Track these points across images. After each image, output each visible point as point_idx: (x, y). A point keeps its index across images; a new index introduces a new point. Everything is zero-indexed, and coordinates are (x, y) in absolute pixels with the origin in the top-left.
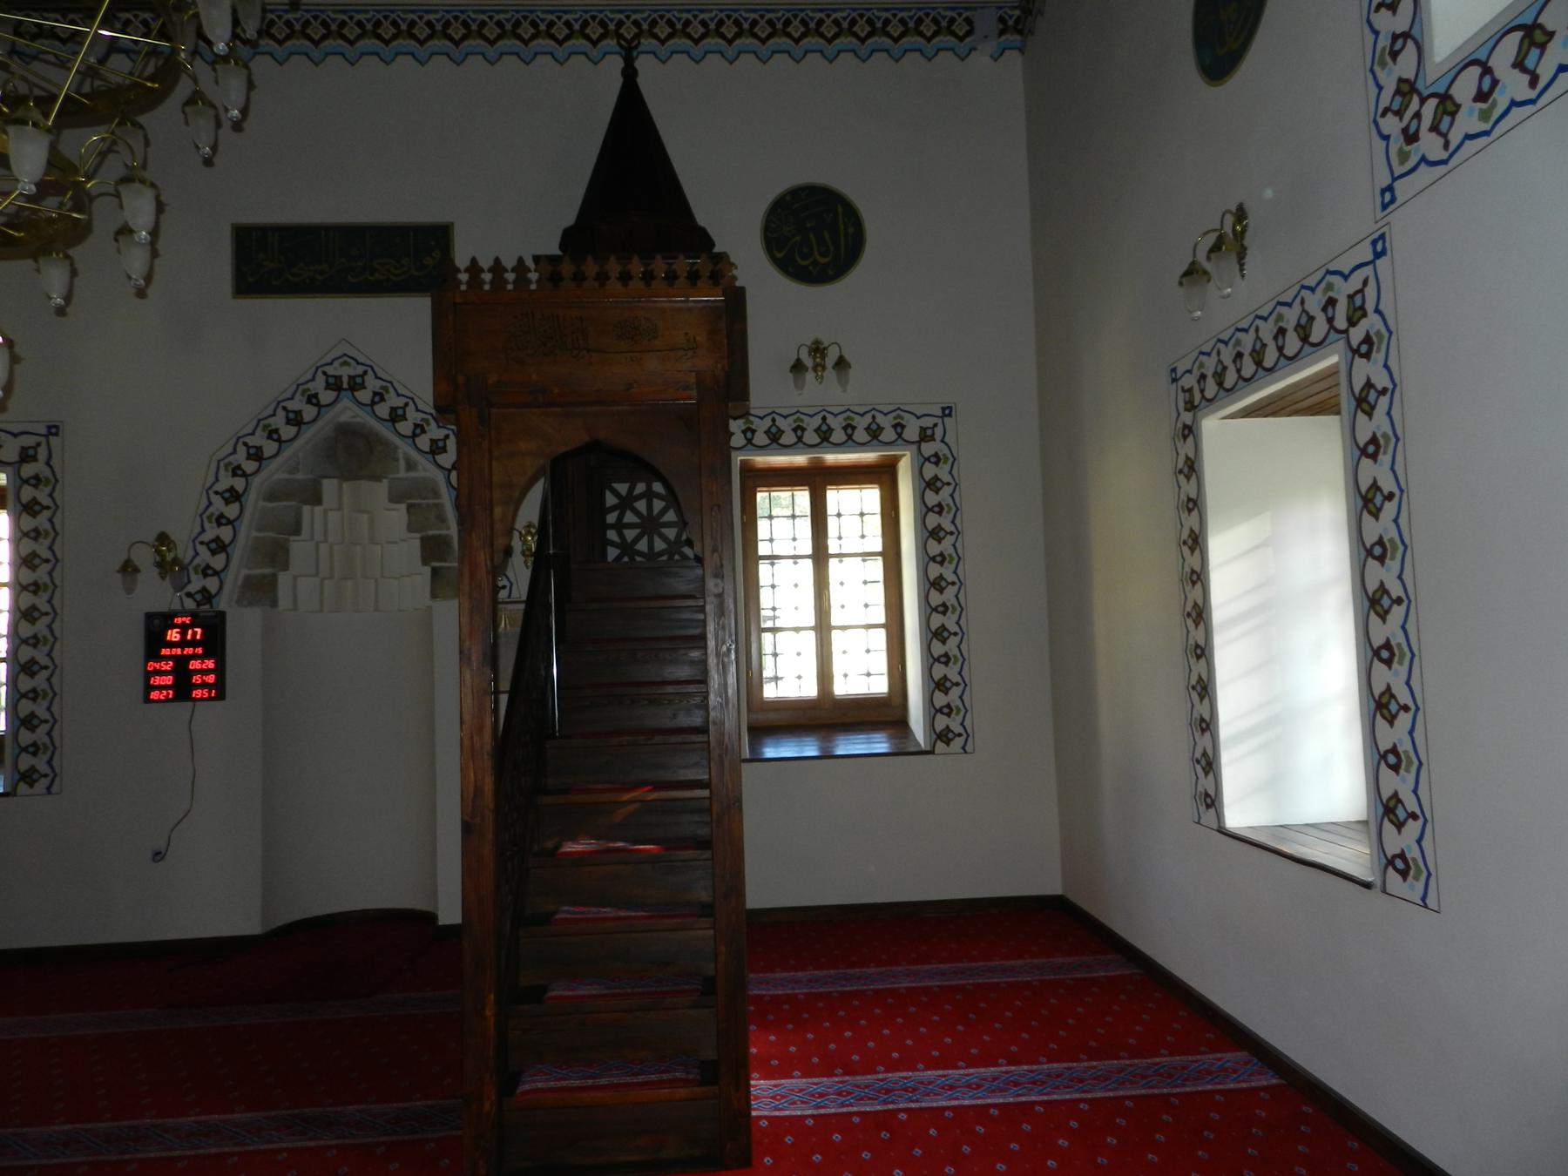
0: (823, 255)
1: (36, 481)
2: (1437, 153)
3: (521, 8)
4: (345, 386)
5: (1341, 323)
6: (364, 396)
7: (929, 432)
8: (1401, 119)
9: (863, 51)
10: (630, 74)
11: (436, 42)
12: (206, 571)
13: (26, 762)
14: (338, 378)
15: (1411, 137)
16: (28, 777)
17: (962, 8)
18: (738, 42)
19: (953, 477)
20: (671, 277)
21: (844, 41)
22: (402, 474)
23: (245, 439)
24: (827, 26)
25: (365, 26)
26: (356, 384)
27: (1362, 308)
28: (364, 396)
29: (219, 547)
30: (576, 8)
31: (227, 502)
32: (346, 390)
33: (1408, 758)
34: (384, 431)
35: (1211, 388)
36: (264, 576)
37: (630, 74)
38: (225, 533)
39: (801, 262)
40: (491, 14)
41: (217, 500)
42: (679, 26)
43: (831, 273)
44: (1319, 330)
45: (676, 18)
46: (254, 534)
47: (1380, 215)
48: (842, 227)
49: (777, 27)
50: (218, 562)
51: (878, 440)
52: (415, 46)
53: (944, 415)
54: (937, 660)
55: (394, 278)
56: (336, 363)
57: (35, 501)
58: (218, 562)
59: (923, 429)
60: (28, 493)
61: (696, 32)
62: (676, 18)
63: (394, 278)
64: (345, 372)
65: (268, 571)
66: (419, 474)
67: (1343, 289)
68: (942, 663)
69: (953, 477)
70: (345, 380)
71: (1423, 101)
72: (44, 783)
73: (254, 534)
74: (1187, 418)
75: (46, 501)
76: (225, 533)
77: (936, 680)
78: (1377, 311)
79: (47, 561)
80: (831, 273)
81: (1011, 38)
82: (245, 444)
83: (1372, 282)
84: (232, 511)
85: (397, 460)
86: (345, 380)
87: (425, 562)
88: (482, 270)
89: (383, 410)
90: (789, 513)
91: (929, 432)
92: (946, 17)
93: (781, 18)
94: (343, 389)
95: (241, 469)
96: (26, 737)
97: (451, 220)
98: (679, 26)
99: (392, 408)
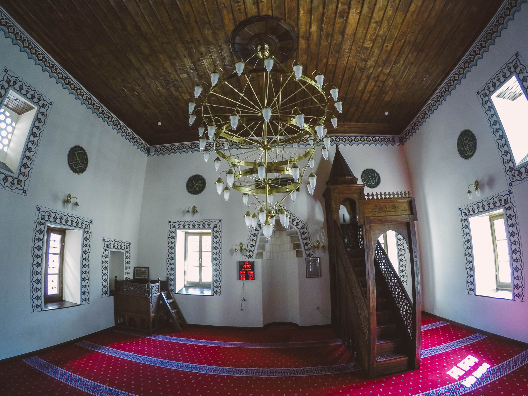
0: (373, 182)
1: (217, 232)
2: (519, 179)
5: (503, 203)
7: (216, 226)
10: (337, 148)
12: (250, 251)
13: (215, 289)
15: (514, 176)
16: (216, 292)
18: (352, 142)
27: (508, 201)
29: (252, 246)
33: (519, 260)
35: (471, 212)
36: (261, 252)
37: (337, 148)
38: (254, 243)
41: (252, 236)
42: (341, 139)
44: (498, 204)
46: (259, 243)
47: (509, 187)
50: (252, 249)
57: (216, 236)
58: (252, 249)
59: (173, 227)
60: (215, 234)
65: (262, 251)
66: (293, 230)
67: (503, 199)
71: (515, 171)
72: (219, 294)
73: (259, 243)
74: (465, 218)
75: (218, 236)
76: (254, 243)
78: (511, 202)
79: (219, 248)
83: (509, 197)
84: (255, 238)
87: (294, 249)
88: (391, 194)
90: (273, 243)
91: (216, 226)
96: (215, 284)
98: (341, 139)
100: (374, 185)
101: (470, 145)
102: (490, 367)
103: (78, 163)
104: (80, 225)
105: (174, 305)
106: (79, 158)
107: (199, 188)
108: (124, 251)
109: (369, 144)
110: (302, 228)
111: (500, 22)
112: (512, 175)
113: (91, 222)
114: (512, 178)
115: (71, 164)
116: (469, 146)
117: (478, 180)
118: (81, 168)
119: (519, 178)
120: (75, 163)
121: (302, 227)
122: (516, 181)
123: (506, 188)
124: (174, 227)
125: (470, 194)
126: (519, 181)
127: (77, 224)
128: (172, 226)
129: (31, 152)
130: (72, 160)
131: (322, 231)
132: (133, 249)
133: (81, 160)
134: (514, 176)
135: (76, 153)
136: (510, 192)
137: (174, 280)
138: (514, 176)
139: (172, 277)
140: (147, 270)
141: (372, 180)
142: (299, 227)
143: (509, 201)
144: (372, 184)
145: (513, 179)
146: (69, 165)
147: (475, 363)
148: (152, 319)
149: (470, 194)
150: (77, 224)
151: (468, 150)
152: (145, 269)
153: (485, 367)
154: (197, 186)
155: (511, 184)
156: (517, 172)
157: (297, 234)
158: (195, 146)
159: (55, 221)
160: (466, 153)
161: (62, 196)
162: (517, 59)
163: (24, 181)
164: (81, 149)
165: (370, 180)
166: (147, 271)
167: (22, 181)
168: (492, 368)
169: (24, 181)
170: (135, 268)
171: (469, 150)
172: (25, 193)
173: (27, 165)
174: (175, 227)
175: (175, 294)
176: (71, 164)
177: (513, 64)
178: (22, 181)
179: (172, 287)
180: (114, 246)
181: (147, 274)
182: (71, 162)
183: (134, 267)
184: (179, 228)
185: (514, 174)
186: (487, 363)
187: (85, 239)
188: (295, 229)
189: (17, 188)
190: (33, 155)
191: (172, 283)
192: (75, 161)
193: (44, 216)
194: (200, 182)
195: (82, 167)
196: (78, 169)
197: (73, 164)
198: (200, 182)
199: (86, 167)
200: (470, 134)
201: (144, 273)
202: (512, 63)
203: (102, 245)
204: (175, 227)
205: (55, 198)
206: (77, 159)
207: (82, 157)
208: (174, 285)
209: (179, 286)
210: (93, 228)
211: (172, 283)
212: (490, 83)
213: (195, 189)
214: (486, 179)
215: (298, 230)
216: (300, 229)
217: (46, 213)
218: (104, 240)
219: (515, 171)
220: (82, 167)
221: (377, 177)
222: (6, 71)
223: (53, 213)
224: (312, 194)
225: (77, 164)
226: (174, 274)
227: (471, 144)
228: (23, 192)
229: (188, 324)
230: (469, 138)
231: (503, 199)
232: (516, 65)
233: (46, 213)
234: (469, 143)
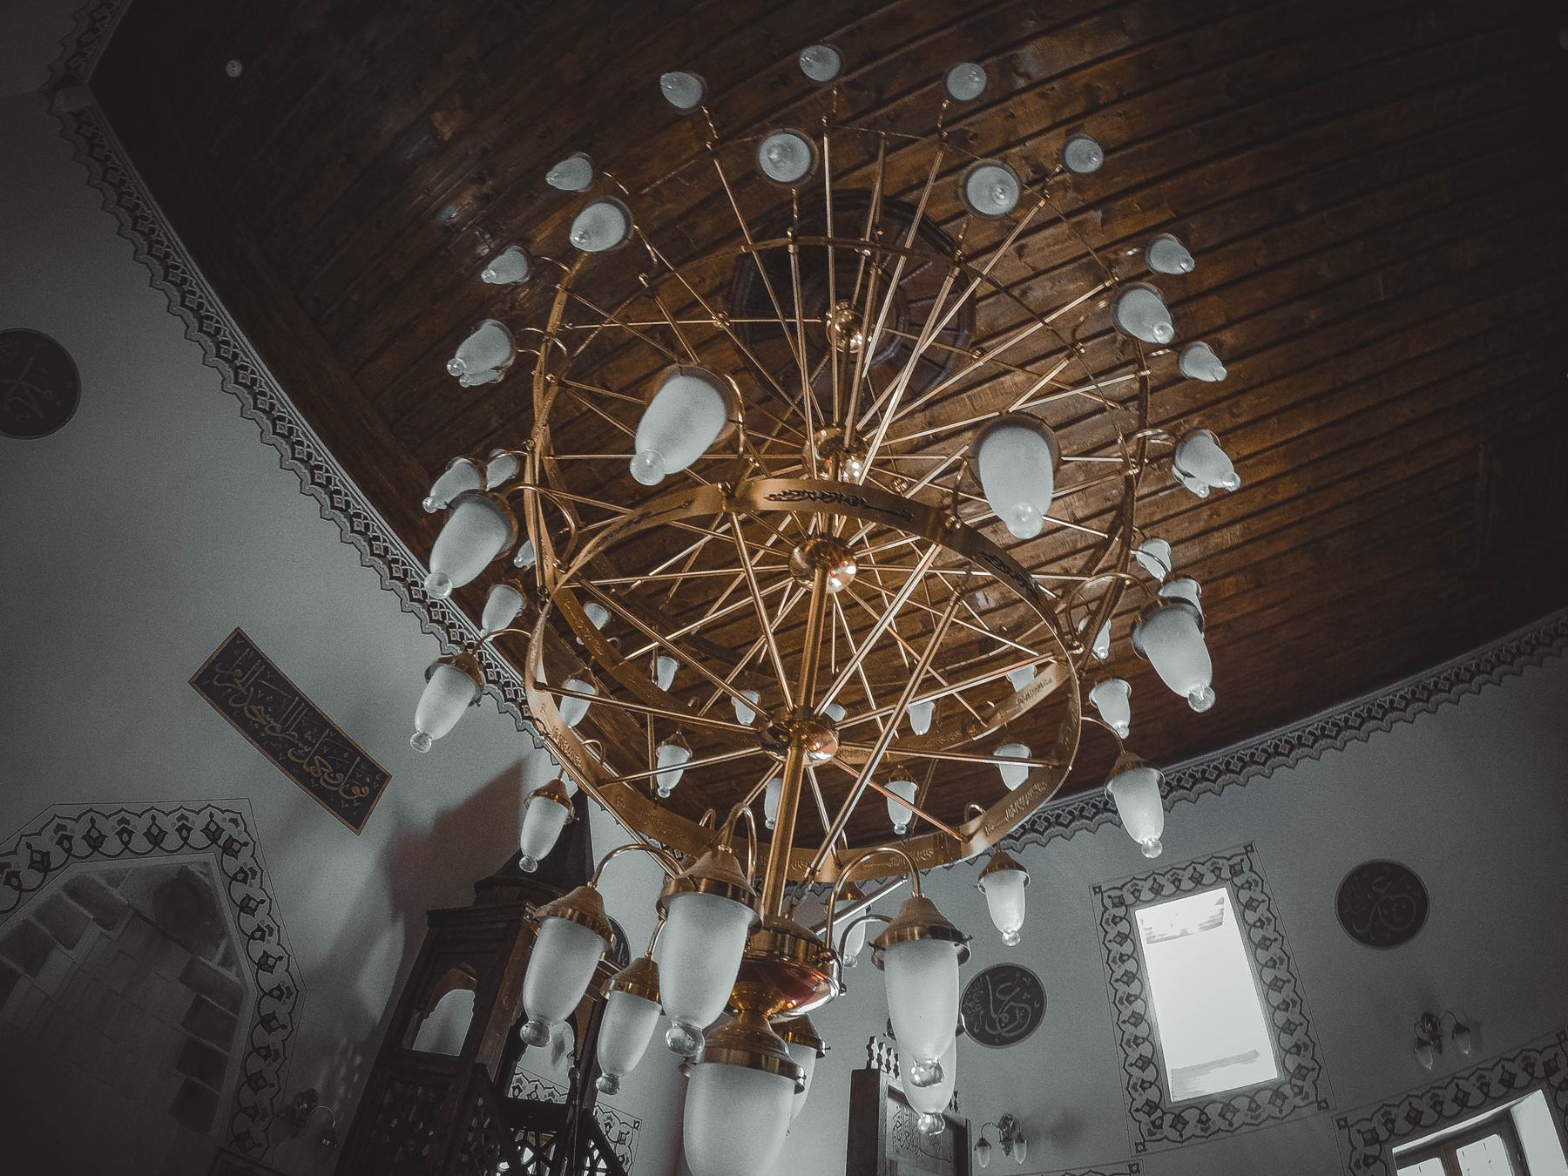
4: (220, 843)
6: (232, 865)
8: (1150, 1116)
14: (220, 830)
19: (1188, 866)
20: (246, 906)
22: (213, 964)
23: (96, 816)
25: (369, 531)
26: (230, 849)
28: (232, 865)
31: (1143, 1069)
32: (219, 846)
34: (229, 914)
46: (32, 919)
47: (1140, 1163)
53: (1247, 852)
55: (324, 784)
56: (228, 816)
63: (324, 784)
64: (229, 830)
66: (230, 974)
69: (1188, 866)
70: (225, 837)
71: (1164, 1113)
73: (32, 919)
82: (93, 821)
85: (218, 946)
86: (225, 837)
89: (240, 891)
93: (209, 312)
94: (217, 844)
95: (1393, 1124)
99: (1406, 1118)
110: (276, 993)
111: (1061, 820)
116: (1011, 1011)
121: (279, 988)
125: (983, 1151)
126: (1170, 1140)
131: (353, 1059)
138: (1156, 1126)
142: (268, 979)
143: (1118, 893)
149: (983, 1151)
155: (1141, 1147)
156: (1169, 1118)
157: (236, 1005)
162: (1105, 894)
171: (1007, 1025)
177: (1231, 862)
188: (240, 974)
202: (1228, 859)
212: (1184, 869)
215: (253, 994)
216: (265, 994)
219: (1164, 1113)
224: (530, 861)
227: (1020, 1009)
232: (1238, 868)
234: (1015, 1005)
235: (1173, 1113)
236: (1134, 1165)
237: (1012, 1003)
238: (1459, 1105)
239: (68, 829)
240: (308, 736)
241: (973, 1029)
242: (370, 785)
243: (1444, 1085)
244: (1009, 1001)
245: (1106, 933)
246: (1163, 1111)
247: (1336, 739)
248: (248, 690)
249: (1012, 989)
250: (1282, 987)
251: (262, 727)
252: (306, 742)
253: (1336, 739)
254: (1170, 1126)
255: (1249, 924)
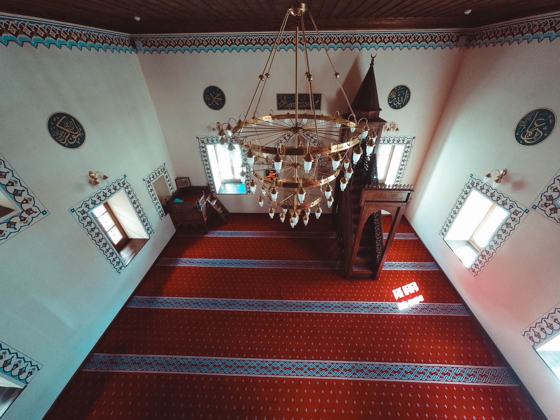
0: (400, 103)
3: (260, 35)
5: (122, 185)
8: (546, 201)
9: (262, 49)
11: (192, 46)
17: (439, 32)
21: (249, 45)
24: (286, 40)
30: (191, 36)
39: (394, 104)
40: (188, 38)
43: (400, 107)
45: (249, 38)
48: (406, 96)
49: (168, 43)
51: (91, 221)
52: (156, 48)
54: (497, 200)
61: (205, 44)
62: (249, 38)
67: (121, 182)
68: (499, 200)
71: (552, 204)
77: (502, 204)
78: (519, 218)
80: (400, 107)
81: (250, 46)
83: (125, 180)
92: (367, 36)
93: (409, 36)
97: (276, 94)
100: (399, 105)
101: (537, 133)
102: (423, 302)
103: (71, 134)
104: (118, 187)
105: (219, 204)
106: (67, 128)
107: (219, 102)
108: (163, 174)
109: (336, 48)
112: (546, 203)
113: (125, 176)
114: (542, 204)
115: (64, 143)
116: (534, 133)
117: (508, 172)
118: (79, 137)
119: (548, 212)
120: (69, 138)
122: (543, 210)
123: (528, 206)
124: (203, 142)
127: (115, 188)
128: (200, 141)
129: (6, 175)
130: (62, 137)
132: (168, 168)
133: (70, 128)
134: (547, 206)
135: (57, 125)
136: (527, 211)
137: (213, 184)
139: (212, 183)
140: (187, 179)
141: (400, 99)
144: (398, 104)
145: (542, 206)
146: (64, 145)
147: (414, 292)
148: (205, 223)
150: (115, 188)
151: (528, 135)
152: (185, 179)
153: (421, 298)
154: (216, 100)
155: (534, 207)
158: (330, 39)
159: (119, 262)
160: (524, 137)
161: (84, 180)
163: (33, 206)
164: (60, 115)
165: (397, 99)
166: (188, 180)
167: (31, 208)
168: (424, 303)
169: (33, 206)
170: (176, 180)
171: (529, 137)
172: (46, 213)
173: (18, 191)
174: (204, 143)
175: (217, 194)
176: (64, 143)
178: (31, 208)
179: (213, 190)
180: (153, 177)
181: (188, 182)
182: (63, 141)
183: (175, 180)
184: (208, 143)
185: (547, 205)
186: (423, 297)
187: (129, 193)
189: (33, 218)
190: (13, 176)
191: (212, 187)
192: (66, 135)
193: (83, 210)
194: (219, 95)
195: (79, 135)
196: (77, 140)
197: (67, 141)
198: (219, 95)
199: (83, 131)
200: (551, 121)
201: (186, 182)
203: (145, 184)
204: (204, 143)
205: (79, 187)
206: (65, 131)
207: (69, 123)
208: (214, 188)
209: (218, 187)
210: (130, 180)
211: (212, 187)
213: (214, 103)
214: (516, 179)
217: (81, 207)
218: (144, 180)
220: (79, 135)
221: (407, 96)
222: (527, 211)
223: (117, 269)
225: (71, 137)
226: (212, 181)
227: (539, 133)
228: (44, 214)
229: (230, 213)
230: (544, 124)
231: (121, 182)
233: (81, 207)
234: (539, 131)
235: (555, 206)
236: (534, 208)
237: (537, 129)
238: (14, 192)
239: (21, 364)
240: (301, 100)
241: (517, 133)
242: (318, 99)
243: (526, 332)
244: (537, 128)
245: (107, 255)
246: (553, 202)
247: (254, 46)
248: (286, 102)
249: (542, 122)
250: (509, 227)
251: (293, 106)
252: (302, 101)
253: (254, 46)
254: (550, 209)
255: (485, 193)
